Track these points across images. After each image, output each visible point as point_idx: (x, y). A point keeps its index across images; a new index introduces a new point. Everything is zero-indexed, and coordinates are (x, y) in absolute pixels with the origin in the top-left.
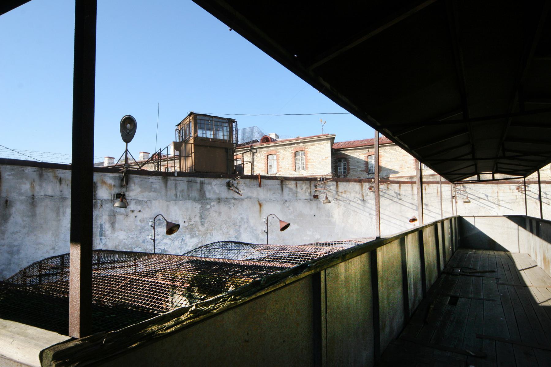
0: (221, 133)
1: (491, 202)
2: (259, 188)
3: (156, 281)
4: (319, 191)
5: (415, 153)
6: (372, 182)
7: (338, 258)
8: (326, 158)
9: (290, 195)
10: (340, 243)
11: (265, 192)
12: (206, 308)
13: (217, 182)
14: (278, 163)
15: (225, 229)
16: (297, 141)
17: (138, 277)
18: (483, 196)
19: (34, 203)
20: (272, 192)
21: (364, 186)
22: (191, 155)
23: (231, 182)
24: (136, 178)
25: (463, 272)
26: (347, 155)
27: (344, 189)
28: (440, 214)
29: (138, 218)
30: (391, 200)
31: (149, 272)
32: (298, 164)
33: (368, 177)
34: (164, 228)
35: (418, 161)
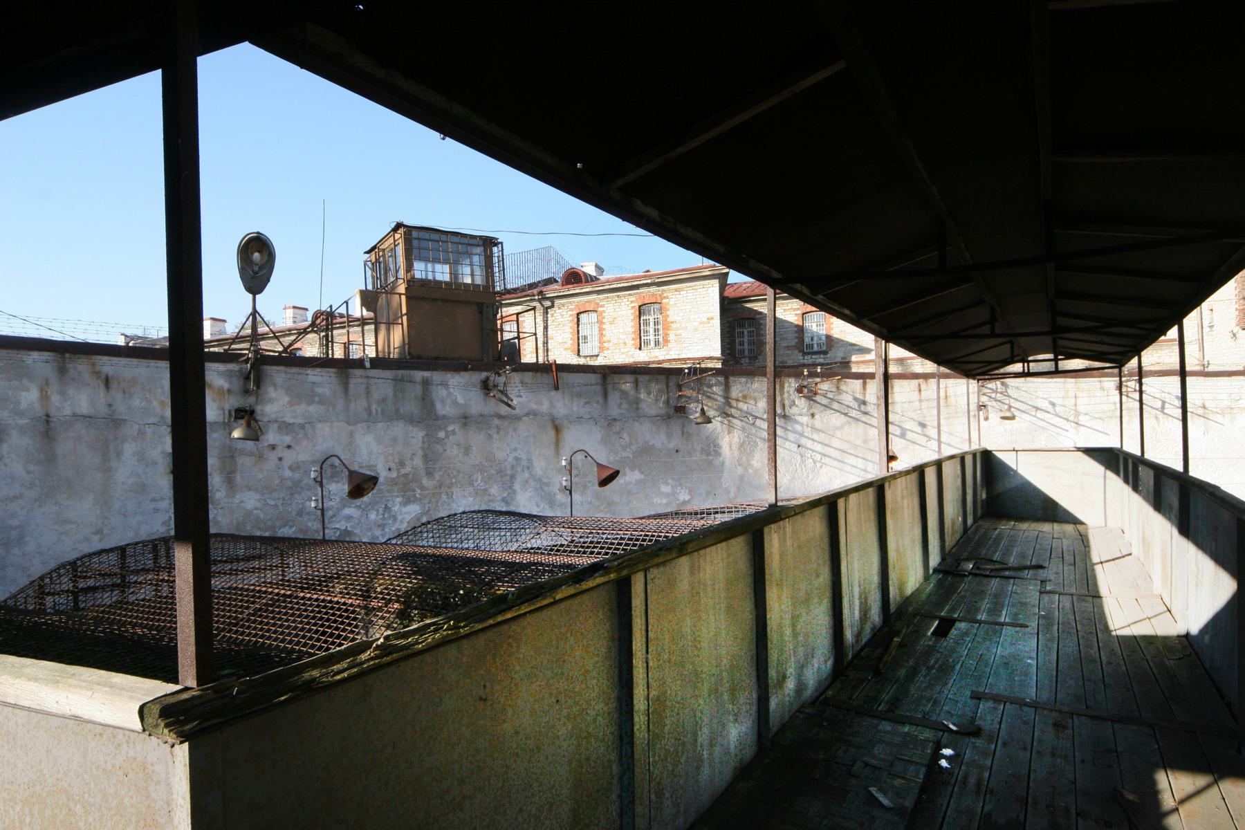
0: (467, 270)
1: (1060, 417)
2: (553, 393)
3: (329, 598)
4: (686, 397)
5: (869, 323)
6: (804, 376)
7: (669, 549)
9: (622, 407)
10: (726, 510)
11: (566, 400)
12: (402, 642)
13: (461, 380)
14: (601, 330)
15: (479, 482)
16: (645, 282)
17: (290, 590)
18: (1040, 403)
20: (583, 401)
21: (786, 385)
23: (492, 379)
24: (277, 374)
25: (978, 568)
26: (756, 311)
28: (937, 449)
29: (286, 463)
30: (846, 414)
31: (312, 580)
33: (802, 361)
34: (344, 484)
35: (879, 339)
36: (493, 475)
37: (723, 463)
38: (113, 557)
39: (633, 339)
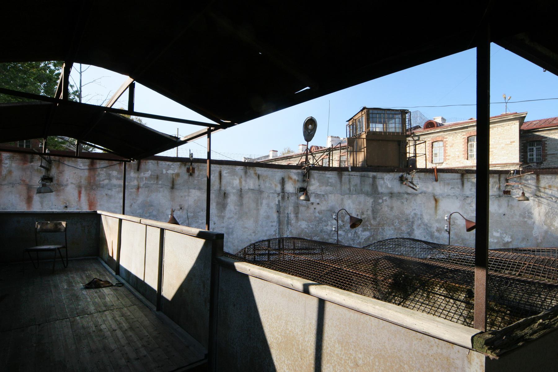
2: (435, 183)
8: (511, 142)
9: (472, 190)
11: (441, 186)
13: (390, 176)
14: (445, 150)
16: (472, 124)
19: (242, 195)
20: (450, 187)
22: (363, 150)
24: (315, 173)
26: (542, 136)
27: (547, 183)
29: (317, 210)
32: (472, 151)
36: (403, 221)
37: (534, 223)
38: (266, 243)
39: (464, 154)
